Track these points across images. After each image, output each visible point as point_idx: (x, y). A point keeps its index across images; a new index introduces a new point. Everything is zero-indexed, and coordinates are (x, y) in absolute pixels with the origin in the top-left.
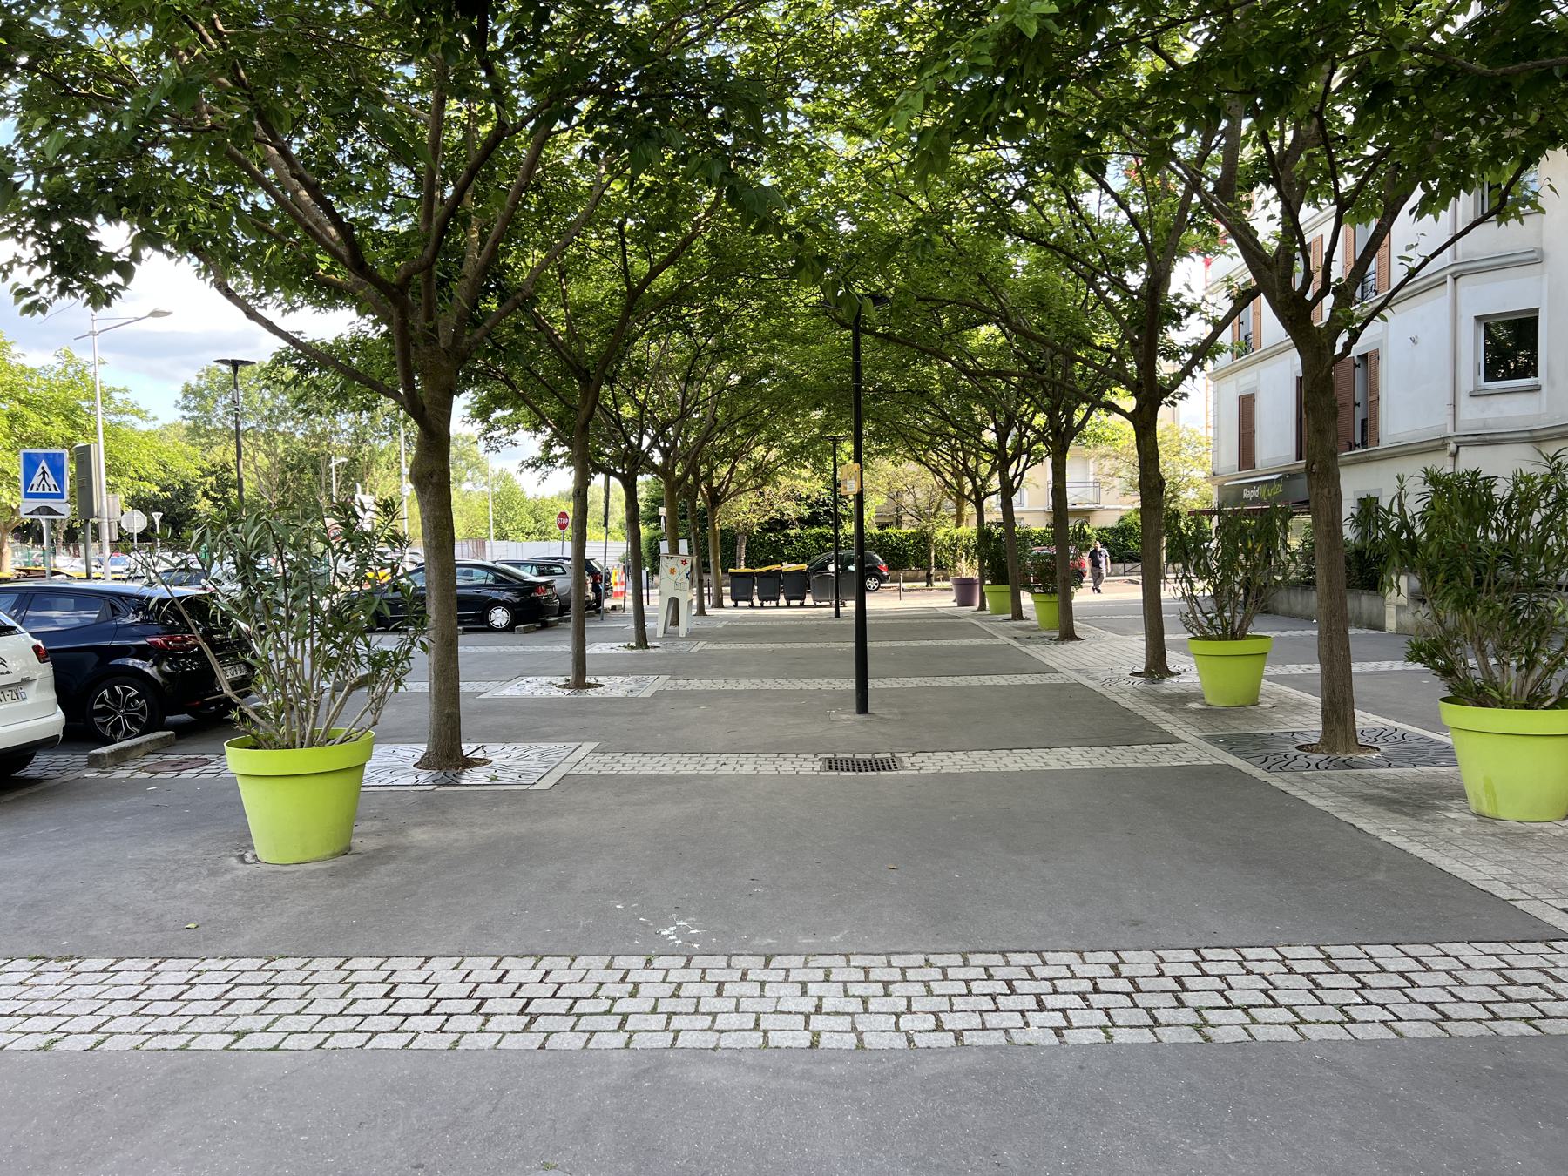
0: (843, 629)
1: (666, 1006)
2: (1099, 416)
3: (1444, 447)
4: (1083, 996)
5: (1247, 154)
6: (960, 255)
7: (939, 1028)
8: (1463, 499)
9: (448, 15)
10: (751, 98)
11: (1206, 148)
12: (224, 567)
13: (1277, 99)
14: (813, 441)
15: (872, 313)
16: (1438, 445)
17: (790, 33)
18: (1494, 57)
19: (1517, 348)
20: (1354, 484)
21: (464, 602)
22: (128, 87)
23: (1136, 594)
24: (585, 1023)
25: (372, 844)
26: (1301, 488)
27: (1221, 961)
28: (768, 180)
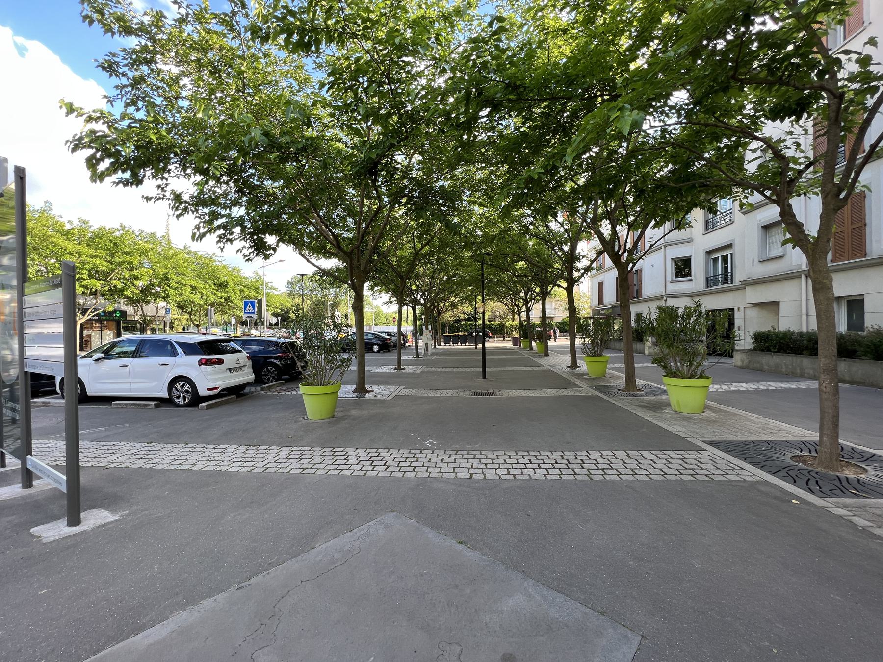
0: (478, 353)
1: (426, 465)
2: (556, 288)
3: (662, 298)
4: (552, 465)
5: (600, 210)
6: (513, 241)
7: (509, 473)
8: (669, 314)
9: (365, 176)
10: (451, 196)
11: (588, 209)
12: (300, 334)
13: (608, 195)
14: (469, 296)
15: (487, 258)
16: (660, 298)
17: (463, 177)
18: (677, 181)
19: (685, 268)
20: (634, 309)
21: (367, 344)
22: (276, 198)
23: (568, 343)
24: (403, 469)
25: (340, 415)
26: (618, 310)
27: (595, 455)
28: (456, 220)
